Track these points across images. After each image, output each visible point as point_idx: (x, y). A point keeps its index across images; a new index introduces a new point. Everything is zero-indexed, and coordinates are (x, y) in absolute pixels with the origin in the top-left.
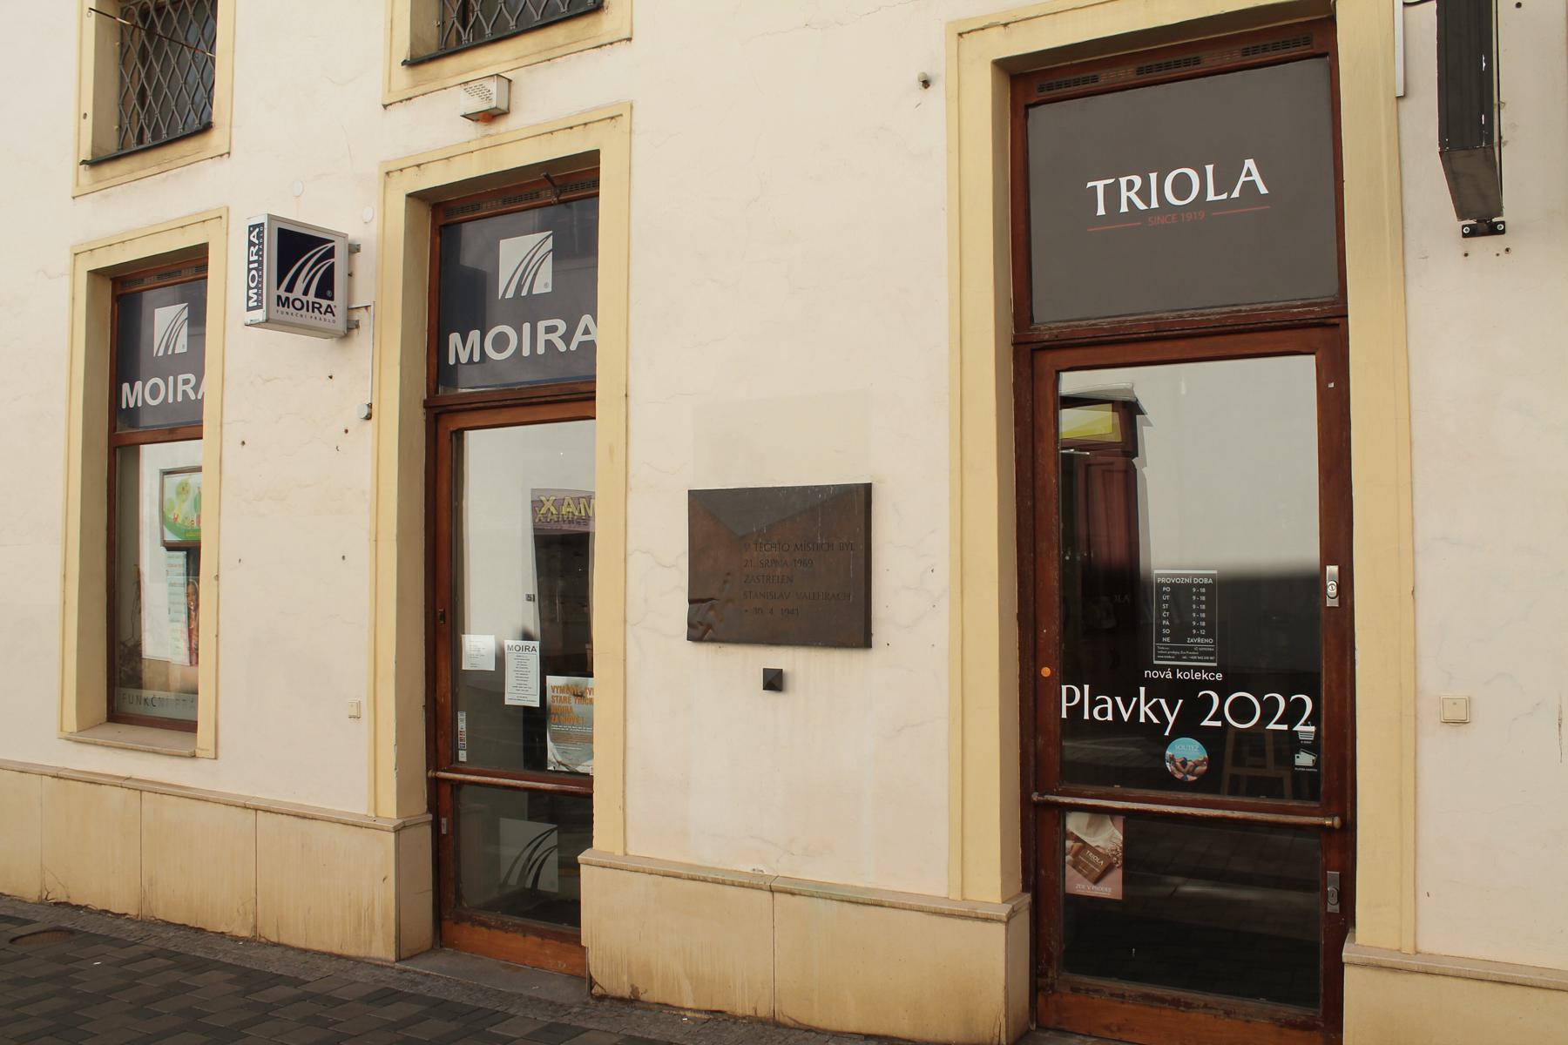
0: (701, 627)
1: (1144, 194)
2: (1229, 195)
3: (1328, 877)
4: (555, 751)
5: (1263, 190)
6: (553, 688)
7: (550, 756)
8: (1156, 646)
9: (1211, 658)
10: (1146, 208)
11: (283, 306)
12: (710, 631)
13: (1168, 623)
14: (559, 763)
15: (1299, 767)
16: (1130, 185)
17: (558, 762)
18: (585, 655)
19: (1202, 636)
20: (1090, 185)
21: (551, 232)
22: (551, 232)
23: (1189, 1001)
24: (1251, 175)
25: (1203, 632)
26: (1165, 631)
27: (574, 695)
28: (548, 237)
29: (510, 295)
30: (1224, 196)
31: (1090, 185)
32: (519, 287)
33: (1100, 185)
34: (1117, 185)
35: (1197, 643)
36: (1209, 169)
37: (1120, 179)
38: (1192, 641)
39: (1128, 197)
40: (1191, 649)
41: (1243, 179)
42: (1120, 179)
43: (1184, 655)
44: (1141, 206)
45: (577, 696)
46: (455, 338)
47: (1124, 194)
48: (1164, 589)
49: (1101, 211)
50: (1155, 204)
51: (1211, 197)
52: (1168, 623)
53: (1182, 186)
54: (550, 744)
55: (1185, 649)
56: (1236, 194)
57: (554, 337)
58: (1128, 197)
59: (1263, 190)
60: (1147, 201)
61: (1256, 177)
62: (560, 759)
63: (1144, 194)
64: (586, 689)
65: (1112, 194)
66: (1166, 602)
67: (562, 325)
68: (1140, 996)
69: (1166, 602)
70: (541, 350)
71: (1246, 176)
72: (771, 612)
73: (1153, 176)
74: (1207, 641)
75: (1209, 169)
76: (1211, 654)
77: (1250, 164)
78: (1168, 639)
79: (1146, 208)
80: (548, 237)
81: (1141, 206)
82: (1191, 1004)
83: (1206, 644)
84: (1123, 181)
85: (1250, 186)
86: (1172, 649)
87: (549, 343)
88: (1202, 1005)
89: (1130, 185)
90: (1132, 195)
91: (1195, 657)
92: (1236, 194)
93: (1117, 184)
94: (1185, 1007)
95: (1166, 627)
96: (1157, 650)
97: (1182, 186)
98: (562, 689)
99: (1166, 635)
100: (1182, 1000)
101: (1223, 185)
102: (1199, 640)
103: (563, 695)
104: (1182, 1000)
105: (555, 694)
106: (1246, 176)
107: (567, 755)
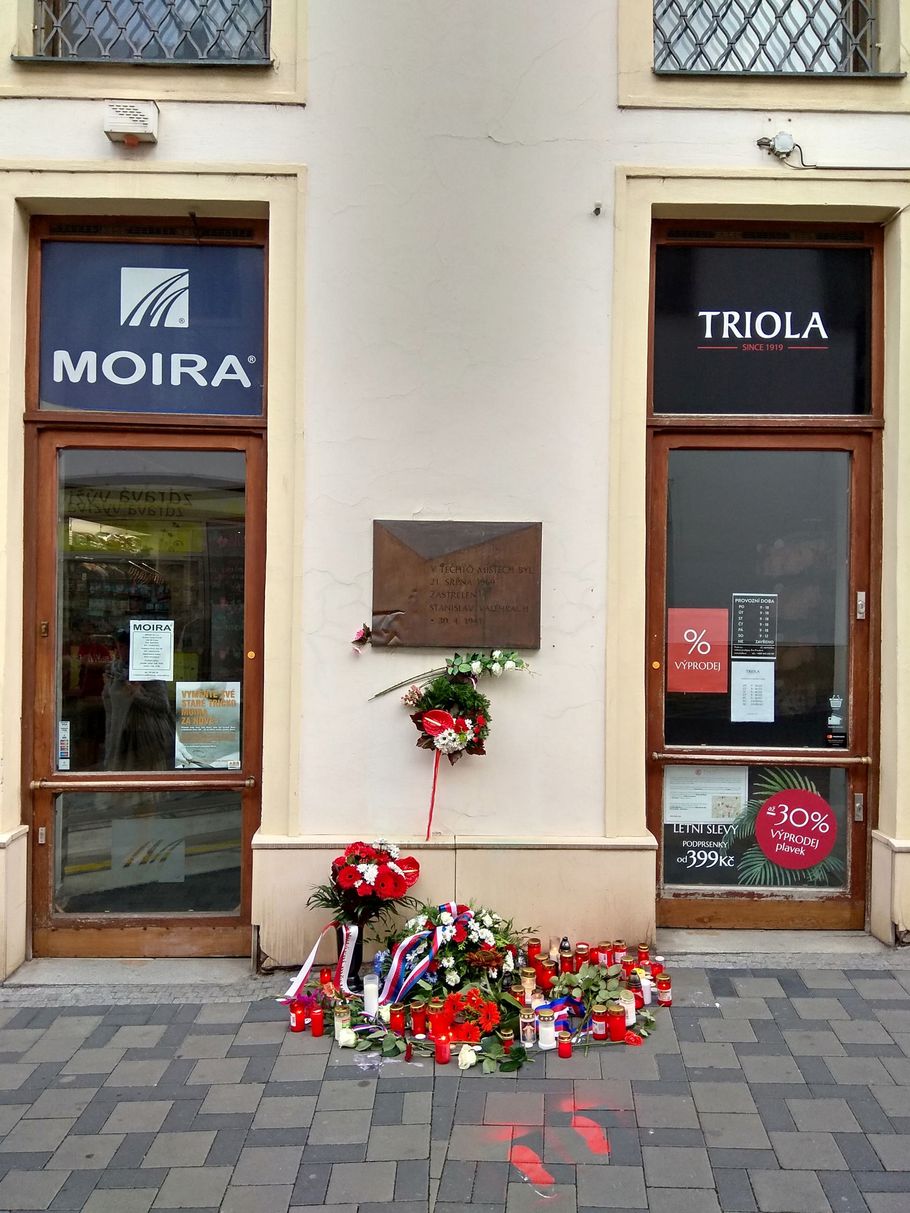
0: (386, 635)
1: (741, 326)
2: (801, 336)
3: (856, 797)
4: (185, 751)
5: (824, 335)
6: (184, 693)
7: (178, 755)
8: (733, 646)
9: (773, 654)
10: (742, 337)
11: (137, 629)
12: (395, 637)
13: (742, 630)
14: (190, 761)
15: (831, 725)
16: (731, 319)
17: (188, 760)
18: (648, 773)
19: (766, 639)
20: (701, 314)
21: (187, 270)
22: (187, 270)
23: (761, 893)
24: (816, 324)
25: (767, 636)
26: (739, 636)
27: (209, 698)
28: (182, 275)
29: (136, 322)
30: (797, 336)
31: (701, 314)
32: (148, 317)
33: (709, 315)
34: (721, 317)
35: (762, 644)
36: (788, 315)
37: (724, 313)
38: (759, 642)
39: (729, 327)
40: (758, 648)
41: (811, 325)
42: (724, 313)
43: (753, 652)
44: (738, 335)
45: (213, 698)
46: (61, 357)
47: (726, 324)
48: (740, 606)
49: (708, 335)
50: (748, 335)
51: (788, 335)
52: (742, 630)
53: (768, 325)
54: (178, 745)
55: (754, 648)
56: (805, 336)
57: (192, 372)
58: (729, 327)
59: (824, 335)
60: (742, 331)
61: (820, 325)
62: (190, 757)
63: (741, 326)
64: (223, 692)
65: (717, 323)
66: (741, 615)
67: (202, 363)
68: (724, 894)
69: (741, 615)
70: (176, 380)
71: (813, 324)
72: (456, 621)
73: (748, 315)
74: (770, 642)
75: (788, 315)
76: (773, 651)
77: (816, 316)
78: (742, 641)
79: (742, 337)
80: (182, 275)
81: (738, 335)
82: (762, 895)
83: (769, 644)
84: (726, 315)
85: (815, 332)
86: (745, 647)
87: (185, 377)
88: (769, 895)
89: (731, 319)
90: (732, 326)
91: (761, 653)
92: (805, 336)
93: (721, 316)
94: (757, 897)
95: (741, 633)
96: (733, 648)
97: (768, 325)
98: (195, 693)
99: (740, 639)
100: (756, 893)
101: (798, 327)
102: (764, 641)
103: (195, 699)
104: (756, 893)
105: (187, 698)
106: (813, 324)
107: (200, 754)
